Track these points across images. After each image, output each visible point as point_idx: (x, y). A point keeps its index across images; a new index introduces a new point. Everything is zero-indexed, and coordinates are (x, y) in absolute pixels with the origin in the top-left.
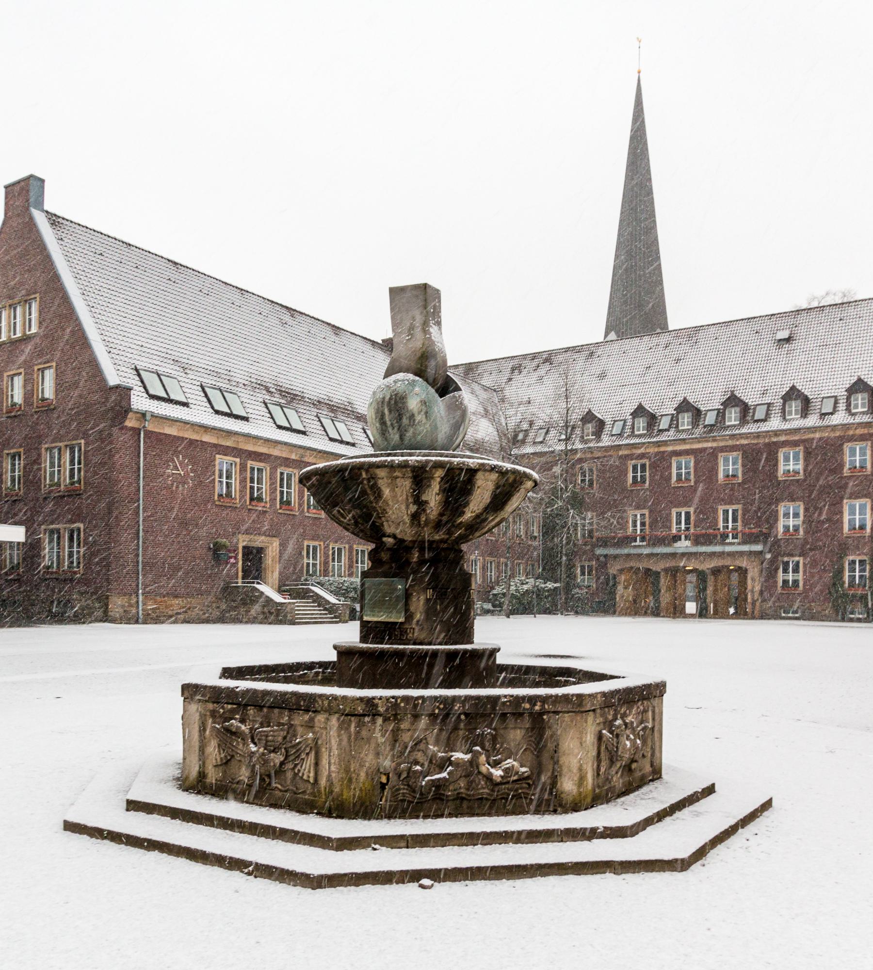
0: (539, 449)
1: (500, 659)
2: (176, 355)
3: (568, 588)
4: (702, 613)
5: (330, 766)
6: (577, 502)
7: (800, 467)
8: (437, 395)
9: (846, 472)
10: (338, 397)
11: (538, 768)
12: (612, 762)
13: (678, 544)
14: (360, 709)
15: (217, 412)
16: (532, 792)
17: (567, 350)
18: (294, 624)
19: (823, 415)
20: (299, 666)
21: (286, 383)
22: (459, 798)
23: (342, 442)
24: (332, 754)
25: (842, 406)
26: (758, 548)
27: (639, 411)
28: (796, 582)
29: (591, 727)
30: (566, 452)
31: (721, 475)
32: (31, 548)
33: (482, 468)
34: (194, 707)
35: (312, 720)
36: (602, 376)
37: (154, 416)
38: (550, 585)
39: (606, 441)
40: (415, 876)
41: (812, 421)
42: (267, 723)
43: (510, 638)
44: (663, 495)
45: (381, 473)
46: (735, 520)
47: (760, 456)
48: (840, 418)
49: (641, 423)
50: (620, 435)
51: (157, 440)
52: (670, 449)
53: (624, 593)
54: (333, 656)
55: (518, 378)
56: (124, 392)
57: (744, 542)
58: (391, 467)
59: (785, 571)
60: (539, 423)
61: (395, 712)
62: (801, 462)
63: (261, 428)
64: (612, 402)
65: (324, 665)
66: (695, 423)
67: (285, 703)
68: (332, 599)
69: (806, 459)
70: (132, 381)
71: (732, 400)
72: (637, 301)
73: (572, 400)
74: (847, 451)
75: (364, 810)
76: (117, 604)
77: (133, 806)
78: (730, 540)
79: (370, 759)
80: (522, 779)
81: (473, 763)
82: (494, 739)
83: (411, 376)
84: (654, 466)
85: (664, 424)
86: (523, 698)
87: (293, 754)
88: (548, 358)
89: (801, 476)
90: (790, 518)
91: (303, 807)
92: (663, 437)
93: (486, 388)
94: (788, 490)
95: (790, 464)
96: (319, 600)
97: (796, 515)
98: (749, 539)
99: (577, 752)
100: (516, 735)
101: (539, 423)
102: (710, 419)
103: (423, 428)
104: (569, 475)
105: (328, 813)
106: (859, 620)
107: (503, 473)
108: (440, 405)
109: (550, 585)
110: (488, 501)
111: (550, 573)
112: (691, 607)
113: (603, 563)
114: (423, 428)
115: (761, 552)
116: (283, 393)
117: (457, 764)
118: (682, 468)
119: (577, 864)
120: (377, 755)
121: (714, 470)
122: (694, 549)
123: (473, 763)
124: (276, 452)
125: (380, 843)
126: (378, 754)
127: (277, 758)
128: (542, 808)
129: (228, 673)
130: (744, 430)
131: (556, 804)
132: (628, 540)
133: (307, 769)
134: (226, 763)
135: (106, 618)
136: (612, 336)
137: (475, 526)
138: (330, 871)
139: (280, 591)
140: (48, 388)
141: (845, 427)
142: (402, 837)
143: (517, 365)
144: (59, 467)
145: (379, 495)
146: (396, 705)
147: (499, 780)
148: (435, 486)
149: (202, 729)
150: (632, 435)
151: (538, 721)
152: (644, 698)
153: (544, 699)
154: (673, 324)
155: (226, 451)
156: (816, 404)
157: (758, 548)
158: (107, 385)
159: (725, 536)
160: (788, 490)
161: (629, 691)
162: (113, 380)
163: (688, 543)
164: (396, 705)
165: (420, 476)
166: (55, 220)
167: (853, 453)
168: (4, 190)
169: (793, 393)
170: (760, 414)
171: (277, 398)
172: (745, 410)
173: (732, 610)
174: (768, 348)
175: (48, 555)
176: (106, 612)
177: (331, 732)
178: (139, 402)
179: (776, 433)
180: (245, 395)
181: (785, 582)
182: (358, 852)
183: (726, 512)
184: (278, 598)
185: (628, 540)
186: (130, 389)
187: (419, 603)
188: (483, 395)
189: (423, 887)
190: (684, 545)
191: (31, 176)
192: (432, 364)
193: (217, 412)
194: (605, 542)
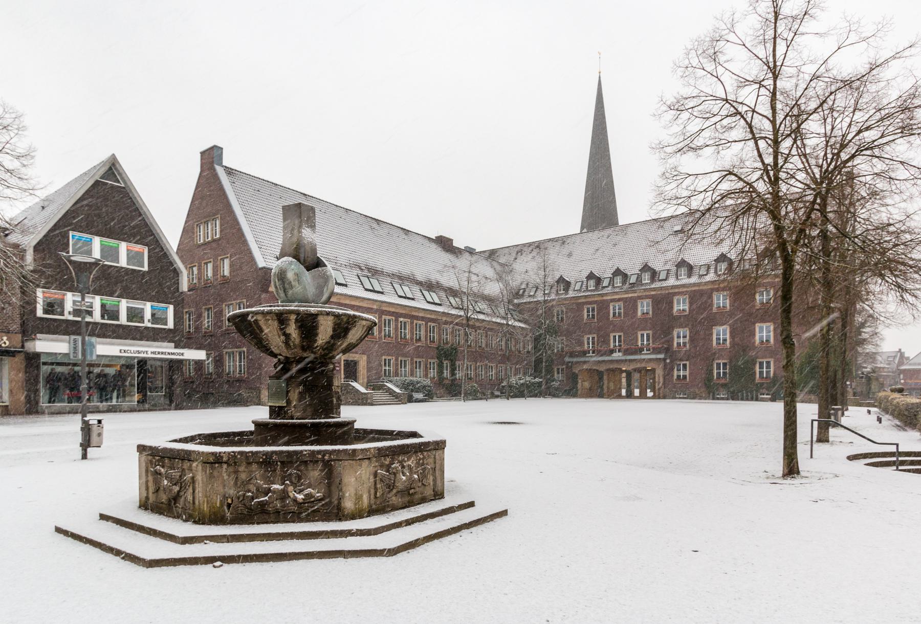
0: (528, 300)
1: (356, 426)
6: (553, 331)
7: (687, 308)
8: (305, 270)
9: (715, 310)
10: (406, 271)
11: (329, 494)
13: (614, 355)
14: (211, 459)
15: (366, 290)
17: (550, 240)
18: (372, 405)
19: (701, 276)
21: (371, 264)
22: (277, 512)
23: (405, 298)
25: (712, 271)
26: (662, 356)
27: (591, 276)
28: (685, 377)
30: (545, 301)
31: (639, 313)
35: (191, 465)
38: (537, 380)
39: (571, 294)
40: (209, 560)
41: (694, 279)
42: (172, 468)
44: (603, 329)
46: (648, 340)
47: (663, 301)
49: (592, 283)
50: (580, 290)
52: (609, 298)
53: (584, 384)
54: (252, 428)
55: (521, 258)
59: (679, 370)
62: (687, 304)
63: (355, 290)
64: (575, 272)
66: (624, 282)
68: (397, 390)
69: (691, 304)
71: (646, 268)
72: (600, 208)
73: (547, 270)
74: (715, 298)
75: (217, 519)
78: (645, 352)
83: (290, 259)
84: (599, 310)
85: (606, 283)
86: (319, 452)
88: (538, 246)
89: (687, 313)
90: (681, 336)
92: (605, 291)
95: (681, 306)
96: (390, 392)
97: (685, 337)
98: (656, 351)
99: (356, 482)
100: (315, 473)
101: (531, 285)
106: (722, 399)
107: (337, 316)
108: (307, 276)
109: (537, 380)
110: (331, 333)
111: (537, 371)
112: (637, 392)
113: (570, 366)
114: (298, 289)
115: (665, 359)
116: (369, 269)
117: (274, 492)
119: (319, 552)
122: (624, 358)
126: (224, 486)
127: (176, 489)
128: (327, 518)
130: (653, 286)
131: (339, 514)
139: (367, 388)
142: (224, 536)
143: (520, 250)
146: (235, 456)
147: (301, 501)
150: (587, 290)
154: (621, 222)
157: (662, 356)
158: (257, 266)
159: (641, 350)
160: (644, 323)
161: (427, 444)
162: (261, 263)
163: (620, 354)
164: (235, 456)
165: (282, 318)
166: (230, 171)
168: (199, 155)
169: (682, 264)
170: (663, 276)
171: (366, 273)
172: (654, 274)
173: (624, 392)
177: (199, 473)
179: (673, 287)
180: (345, 271)
181: (679, 376)
182: (196, 545)
183: (642, 335)
184: (363, 390)
185: (584, 353)
187: (294, 395)
189: (214, 567)
190: (617, 355)
192: (302, 250)
193: (366, 290)
194: (572, 355)
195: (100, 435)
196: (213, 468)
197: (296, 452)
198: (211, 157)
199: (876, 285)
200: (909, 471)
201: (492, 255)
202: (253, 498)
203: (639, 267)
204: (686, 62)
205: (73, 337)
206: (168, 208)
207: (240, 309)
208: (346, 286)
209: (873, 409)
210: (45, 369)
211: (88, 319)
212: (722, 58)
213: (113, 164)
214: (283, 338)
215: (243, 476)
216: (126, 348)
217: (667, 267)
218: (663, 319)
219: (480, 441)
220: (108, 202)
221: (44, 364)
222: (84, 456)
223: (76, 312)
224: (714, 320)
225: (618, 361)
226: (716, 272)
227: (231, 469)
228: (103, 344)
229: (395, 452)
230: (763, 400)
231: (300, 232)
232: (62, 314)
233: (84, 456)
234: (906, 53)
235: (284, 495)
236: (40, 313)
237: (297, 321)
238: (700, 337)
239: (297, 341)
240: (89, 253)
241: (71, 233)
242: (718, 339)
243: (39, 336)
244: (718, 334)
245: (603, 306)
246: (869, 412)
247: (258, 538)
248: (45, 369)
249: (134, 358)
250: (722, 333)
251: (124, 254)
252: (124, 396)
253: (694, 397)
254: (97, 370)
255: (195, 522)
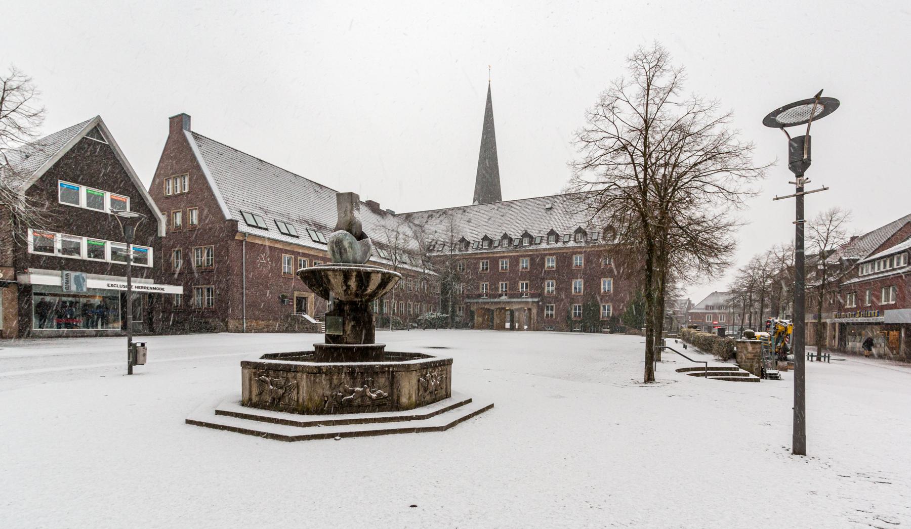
0: (439, 254)
1: (386, 350)
2: (261, 205)
3: (452, 317)
4: (512, 328)
5: (304, 393)
6: (457, 278)
7: (554, 265)
11: (391, 394)
12: (425, 391)
15: (283, 233)
16: (391, 403)
17: (453, 209)
19: (564, 242)
20: (293, 354)
21: (317, 220)
24: (304, 391)
25: (572, 239)
26: (536, 300)
27: (485, 238)
28: (552, 315)
29: (414, 377)
30: (452, 256)
32: (187, 296)
33: (374, 272)
34: (246, 371)
36: (469, 221)
37: (250, 234)
40: (344, 435)
41: (560, 245)
43: (389, 340)
44: (495, 276)
45: (330, 273)
46: (526, 287)
47: (537, 260)
48: (571, 244)
49: (486, 243)
50: (477, 249)
51: (252, 246)
53: (478, 319)
54: (313, 349)
55: (431, 221)
56: (234, 223)
57: (510, 298)
58: (334, 270)
60: (439, 242)
61: (329, 372)
63: (305, 241)
64: (472, 234)
65: (308, 353)
67: (287, 369)
70: (239, 217)
71: (526, 235)
72: (488, 187)
76: (231, 325)
77: (218, 412)
79: (320, 391)
80: (385, 398)
81: (364, 391)
82: (373, 383)
85: (496, 244)
87: (287, 389)
88: (444, 212)
90: (550, 287)
91: (292, 411)
93: (416, 225)
94: (549, 274)
95: (550, 263)
97: (552, 286)
98: (532, 296)
99: (408, 387)
101: (439, 242)
102: (516, 243)
103: (350, 255)
104: (454, 267)
105: (302, 413)
106: (606, 332)
107: (384, 274)
108: (358, 245)
112: (508, 325)
116: (315, 224)
117: (357, 392)
118: (504, 264)
120: (323, 388)
121: (518, 265)
123: (364, 391)
124: (312, 253)
125: (321, 423)
127: (281, 391)
129: (267, 356)
132: (480, 296)
133: (294, 395)
134: (260, 394)
135: (227, 330)
136: (477, 203)
137: (374, 294)
138: (297, 435)
139: (315, 318)
140: (195, 218)
141: (573, 248)
143: (431, 214)
144: (201, 257)
145: (329, 281)
148: (353, 279)
149: (250, 380)
150: (482, 249)
151: (392, 375)
152: (444, 365)
153: (396, 366)
154: (504, 198)
155: (286, 252)
156: (561, 238)
157: (536, 300)
159: (522, 294)
160: (523, 276)
161: (440, 362)
162: (228, 216)
165: (346, 275)
166: (196, 136)
167: (576, 260)
168: (168, 121)
169: (552, 232)
170: (538, 241)
172: (532, 239)
173: (508, 325)
174: (543, 212)
175: (197, 300)
176: (227, 326)
178: (242, 227)
179: (545, 249)
180: (297, 225)
181: (548, 315)
184: (313, 321)
185: (480, 296)
186: (237, 221)
187: (349, 328)
188: (414, 228)
190: (504, 298)
191: (183, 114)
193: (283, 233)
194: (468, 297)
195: (144, 355)
196: (315, 377)
197: (371, 366)
198: (179, 123)
199: (689, 258)
200: (722, 379)
201: (408, 217)
202: (343, 397)
203: (481, 236)
204: (595, 112)
205: (65, 272)
206: (143, 162)
207: (311, 266)
208: (297, 237)
209: (679, 340)
210: (35, 300)
211: (76, 257)
212: (616, 111)
213: (98, 125)
214: (345, 288)
215: (335, 382)
216: (113, 283)
217: (541, 235)
218: (536, 275)
219: (476, 358)
220: (92, 156)
221: (36, 294)
222: (130, 372)
223: (64, 251)
224: (573, 275)
225: (504, 303)
226: (575, 240)
227: (328, 377)
228: (93, 278)
229: (425, 366)
230: (604, 332)
231: (351, 212)
232: (52, 251)
233: (130, 372)
234: (726, 120)
235: (363, 395)
236: (31, 250)
237: (357, 276)
238: (564, 286)
239: (355, 289)
240: (102, 205)
241: (60, 182)
242: (576, 289)
243: (30, 270)
244: (576, 285)
245: (495, 261)
246: (676, 342)
247: (352, 421)
248: (35, 300)
249: (118, 291)
250: (578, 284)
251: (108, 202)
252: (107, 324)
253: (559, 329)
254: (83, 301)
255: (300, 413)
